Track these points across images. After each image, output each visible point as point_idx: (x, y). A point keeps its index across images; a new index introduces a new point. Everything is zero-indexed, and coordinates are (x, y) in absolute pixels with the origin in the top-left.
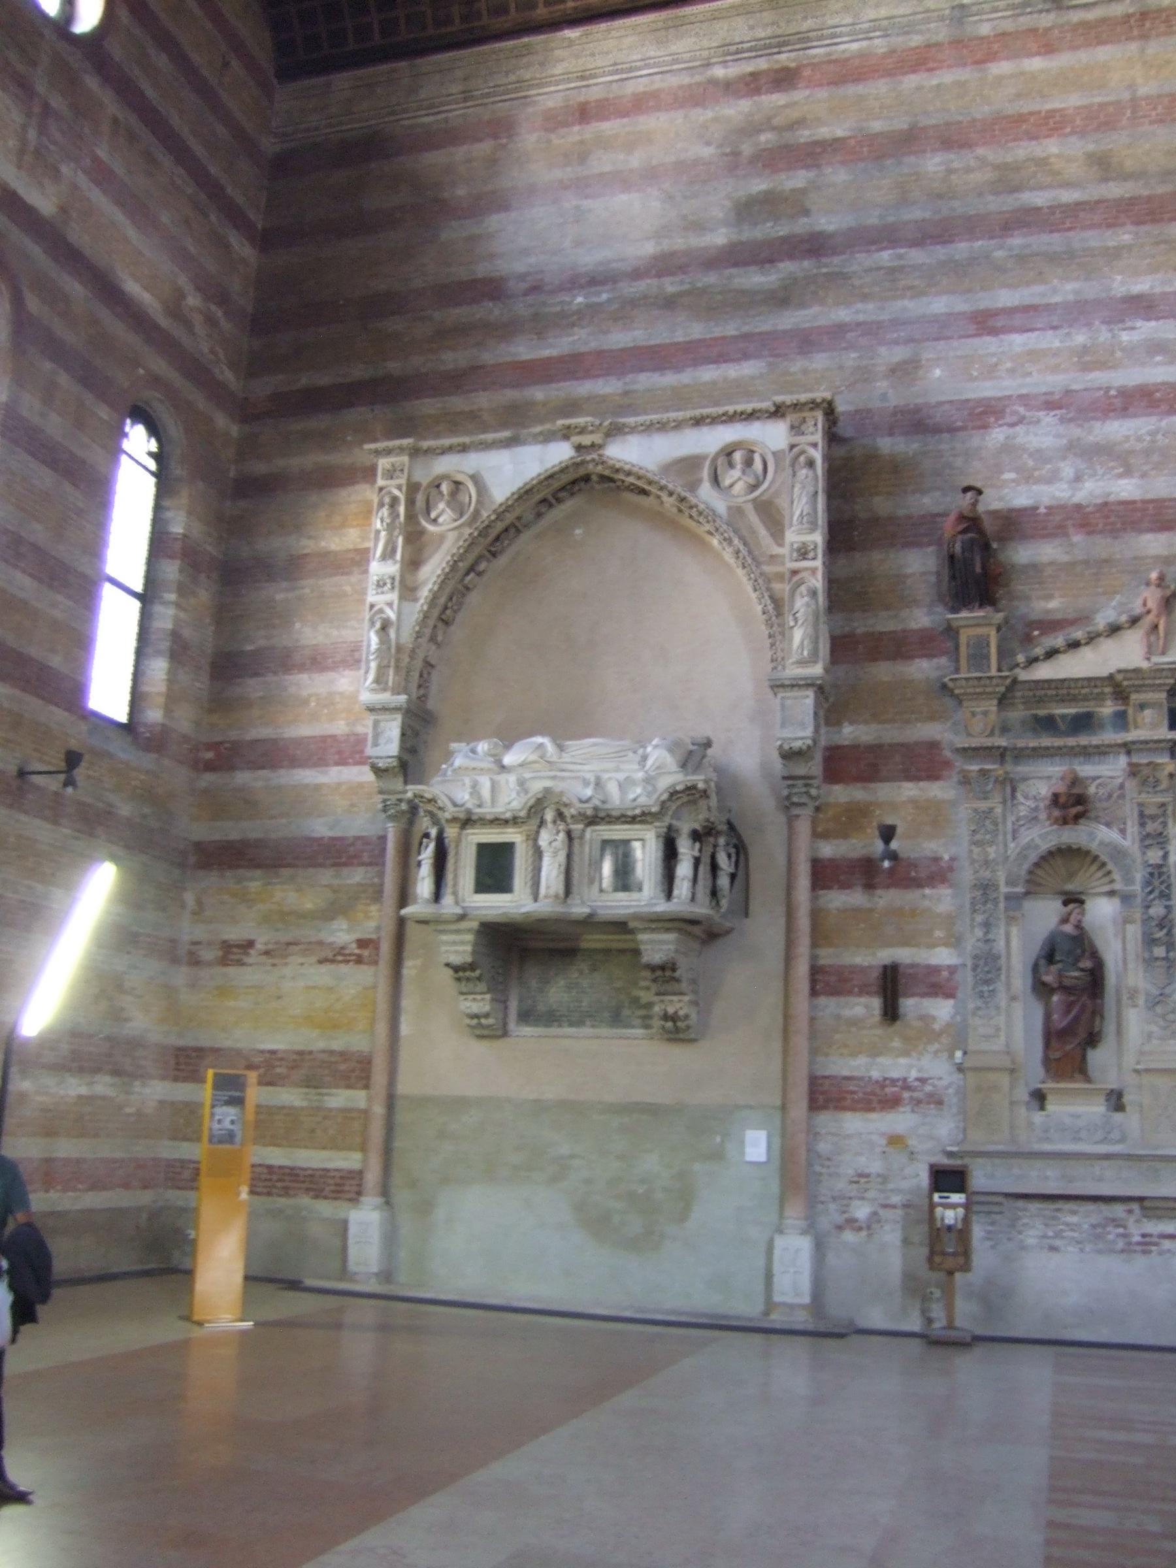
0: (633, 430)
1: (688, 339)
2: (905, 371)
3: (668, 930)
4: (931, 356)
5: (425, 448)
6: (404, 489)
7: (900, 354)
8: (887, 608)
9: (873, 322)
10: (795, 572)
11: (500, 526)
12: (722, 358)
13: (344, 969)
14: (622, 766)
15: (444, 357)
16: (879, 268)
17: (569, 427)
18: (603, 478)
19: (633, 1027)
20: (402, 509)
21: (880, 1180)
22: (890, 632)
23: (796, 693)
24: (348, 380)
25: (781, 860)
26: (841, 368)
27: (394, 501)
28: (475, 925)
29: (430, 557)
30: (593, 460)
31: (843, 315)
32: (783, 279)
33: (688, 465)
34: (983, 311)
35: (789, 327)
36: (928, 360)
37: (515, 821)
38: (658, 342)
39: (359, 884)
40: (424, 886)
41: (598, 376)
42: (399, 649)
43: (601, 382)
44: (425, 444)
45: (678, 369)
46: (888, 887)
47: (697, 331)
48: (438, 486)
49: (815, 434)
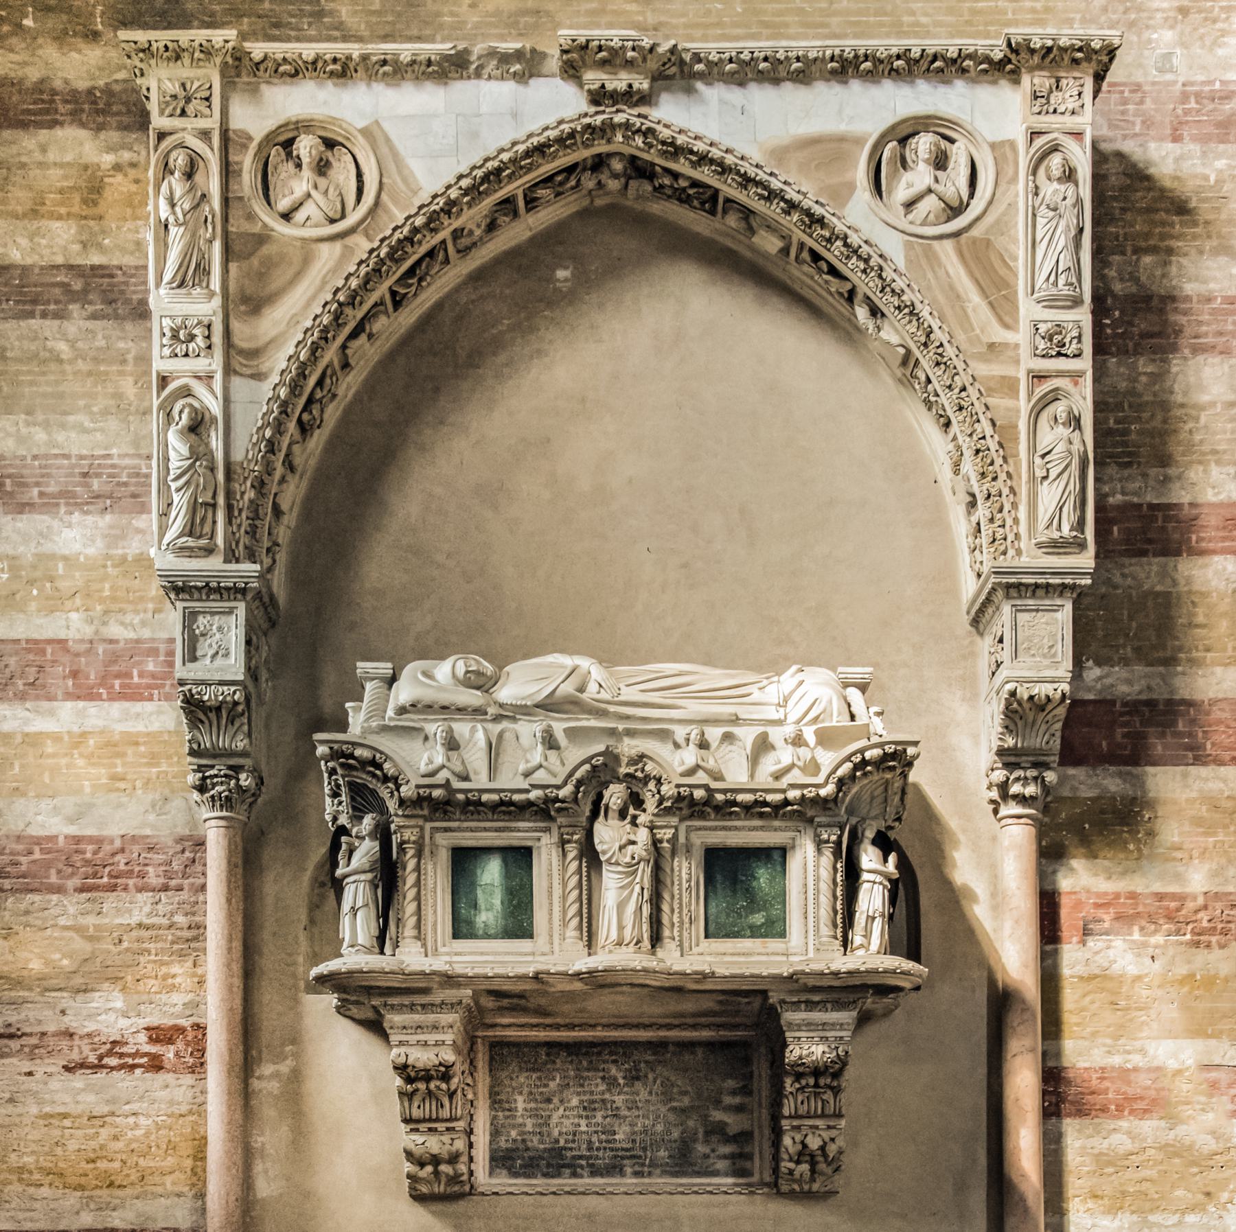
3: (839, 1005)
5: (257, 55)
10: (1039, 377)
13: (124, 1083)
19: (715, 1174)
30: (627, 126)
33: (826, 150)
37: (543, 810)
39: (140, 925)
44: (258, 49)
48: (288, 144)
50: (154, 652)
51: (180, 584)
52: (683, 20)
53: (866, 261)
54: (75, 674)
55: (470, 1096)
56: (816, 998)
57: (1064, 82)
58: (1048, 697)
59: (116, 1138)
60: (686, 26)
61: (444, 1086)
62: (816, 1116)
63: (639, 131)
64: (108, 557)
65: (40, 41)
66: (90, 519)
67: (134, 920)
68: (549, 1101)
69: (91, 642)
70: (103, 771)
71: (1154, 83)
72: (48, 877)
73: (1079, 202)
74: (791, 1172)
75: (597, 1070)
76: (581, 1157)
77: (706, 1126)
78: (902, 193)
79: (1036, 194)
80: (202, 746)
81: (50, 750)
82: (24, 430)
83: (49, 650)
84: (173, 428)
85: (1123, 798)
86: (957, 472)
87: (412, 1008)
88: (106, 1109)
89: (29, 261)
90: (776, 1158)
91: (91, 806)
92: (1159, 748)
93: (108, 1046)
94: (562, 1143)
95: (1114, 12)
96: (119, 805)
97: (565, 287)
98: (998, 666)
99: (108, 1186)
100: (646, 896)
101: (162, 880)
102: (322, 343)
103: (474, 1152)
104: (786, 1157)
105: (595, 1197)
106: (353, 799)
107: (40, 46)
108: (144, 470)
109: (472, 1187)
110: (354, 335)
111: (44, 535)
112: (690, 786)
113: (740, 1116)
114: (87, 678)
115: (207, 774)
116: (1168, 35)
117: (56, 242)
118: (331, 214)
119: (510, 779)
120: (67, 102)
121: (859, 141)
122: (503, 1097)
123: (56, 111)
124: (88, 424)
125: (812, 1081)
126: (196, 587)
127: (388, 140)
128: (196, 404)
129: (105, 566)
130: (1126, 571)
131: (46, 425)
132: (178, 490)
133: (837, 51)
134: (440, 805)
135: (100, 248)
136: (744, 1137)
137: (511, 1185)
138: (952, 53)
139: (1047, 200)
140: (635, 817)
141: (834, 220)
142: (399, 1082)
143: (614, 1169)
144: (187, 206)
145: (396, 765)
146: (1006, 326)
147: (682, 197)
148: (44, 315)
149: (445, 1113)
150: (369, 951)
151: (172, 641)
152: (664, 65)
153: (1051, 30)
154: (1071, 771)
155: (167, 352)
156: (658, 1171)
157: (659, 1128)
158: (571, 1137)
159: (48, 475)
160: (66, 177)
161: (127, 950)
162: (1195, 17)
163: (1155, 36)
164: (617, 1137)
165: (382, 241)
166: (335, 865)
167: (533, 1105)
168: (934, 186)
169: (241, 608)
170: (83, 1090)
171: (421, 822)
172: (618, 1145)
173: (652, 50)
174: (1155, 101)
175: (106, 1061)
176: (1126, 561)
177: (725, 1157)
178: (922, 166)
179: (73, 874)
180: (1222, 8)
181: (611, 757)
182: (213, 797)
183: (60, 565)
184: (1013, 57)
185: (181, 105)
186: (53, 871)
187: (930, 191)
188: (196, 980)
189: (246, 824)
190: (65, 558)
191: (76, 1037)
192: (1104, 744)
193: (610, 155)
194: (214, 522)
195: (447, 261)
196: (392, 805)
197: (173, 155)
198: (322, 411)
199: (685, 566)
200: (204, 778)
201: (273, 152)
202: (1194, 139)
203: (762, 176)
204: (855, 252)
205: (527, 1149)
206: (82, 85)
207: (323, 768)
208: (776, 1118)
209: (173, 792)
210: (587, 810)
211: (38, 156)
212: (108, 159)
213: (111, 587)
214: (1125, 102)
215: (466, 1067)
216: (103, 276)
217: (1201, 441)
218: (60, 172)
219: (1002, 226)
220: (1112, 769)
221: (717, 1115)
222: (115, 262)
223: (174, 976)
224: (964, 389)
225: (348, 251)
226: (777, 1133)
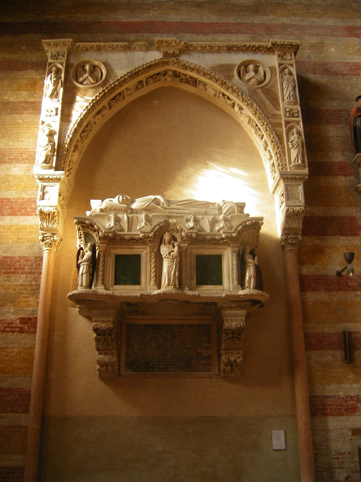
1: (209, 22)
3: (241, 308)
4: (329, 42)
7: (314, 40)
13: (11, 337)
15: (78, 15)
16: (301, 4)
21: (350, 456)
24: (25, 21)
27: (58, 71)
31: (285, 20)
34: (350, 27)
35: (260, 22)
36: (327, 44)
37: (142, 241)
38: (194, 21)
39: (21, 285)
51: (41, 177)
54: (11, 208)
58: (298, 211)
59: (6, 356)
61: (110, 337)
64: (25, 175)
67: (19, 283)
69: (17, 199)
70: (16, 237)
73: (294, 80)
78: (247, 77)
80: (44, 227)
83: (5, 201)
88: (4, 346)
89: (15, 101)
93: (7, 324)
99: (2, 373)
101: (29, 270)
102: (88, 113)
106: (85, 239)
110: (98, 113)
112: (191, 233)
115: (45, 236)
116: (309, 51)
121: (235, 66)
126: (45, 178)
129: (24, 178)
133: (228, 45)
140: (174, 244)
142: (95, 335)
147: (187, 82)
152: (183, 47)
154: (305, 238)
159: (12, 154)
163: (306, 51)
175: (7, 329)
179: (3, 268)
180: (321, 46)
181: (167, 223)
182: (46, 243)
183: (11, 178)
184: (273, 47)
188: (36, 302)
190: (13, 176)
195: (124, 97)
200: (44, 237)
201: (79, 68)
219: (275, 85)
223: (30, 301)
226: (219, 356)
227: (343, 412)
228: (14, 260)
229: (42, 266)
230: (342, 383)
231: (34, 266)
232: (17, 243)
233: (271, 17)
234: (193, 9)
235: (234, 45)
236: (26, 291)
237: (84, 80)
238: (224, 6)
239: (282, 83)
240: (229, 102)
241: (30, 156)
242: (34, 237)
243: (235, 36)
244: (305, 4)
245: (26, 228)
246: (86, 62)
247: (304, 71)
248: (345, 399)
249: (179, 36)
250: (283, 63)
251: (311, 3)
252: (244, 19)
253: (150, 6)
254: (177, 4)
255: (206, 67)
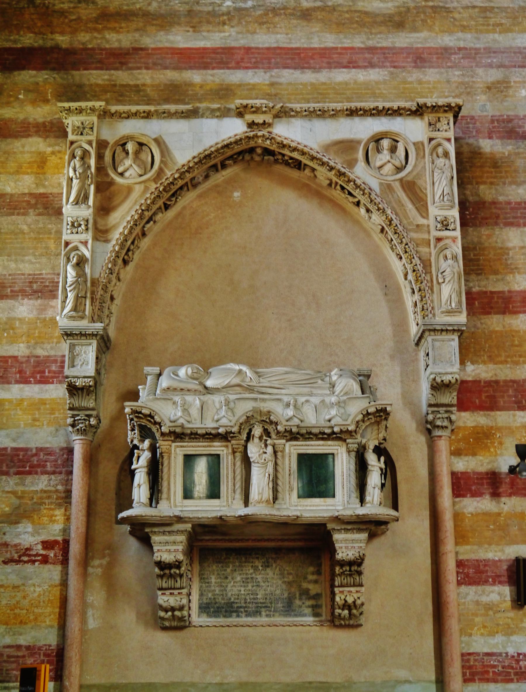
0: (297, 114)
1: (322, 46)
2: (498, 89)
3: (360, 530)
4: (518, 79)
5: (113, 111)
6: (94, 145)
7: (494, 75)
8: (496, 272)
9: (471, 49)
10: (439, 240)
11: (180, 183)
12: (351, 65)
13: (29, 568)
14: (315, 391)
16: (474, 7)
17: (246, 107)
18: (267, 151)
19: (305, 615)
20: (92, 162)
22: (499, 292)
23: (445, 336)
24: (19, 46)
25: (424, 472)
26: (448, 82)
27: (85, 154)
28: (188, 526)
29: (119, 205)
31: (448, 40)
32: (398, 7)
33: (346, 146)
37: (225, 437)
38: (297, 45)
39: (42, 491)
40: (140, 490)
41: (247, 68)
42: (94, 282)
43: (250, 72)
44: (113, 109)
45: (316, 69)
46: (510, 495)
47: (329, 40)
49: (448, 130)
50: (55, 361)
52: (286, 92)
53: (363, 191)
54: (20, 372)
55: (190, 576)
56: (349, 527)
57: (441, 119)
60: (288, 94)
61: (178, 572)
62: (351, 586)
63: (268, 138)
64: (38, 318)
65: (25, 103)
66: (31, 302)
68: (226, 578)
69: (28, 357)
71: (479, 116)
72: (2, 468)
74: (340, 615)
75: (249, 562)
76: (241, 607)
77: (300, 590)
79: (433, 163)
81: (7, 407)
82: (6, 263)
83: (10, 361)
84: (70, 264)
85: (487, 426)
86: (406, 279)
87: (164, 533)
88: (20, 583)
89: (14, 192)
90: (333, 608)
91: (23, 433)
92: (502, 403)
94: (232, 600)
95: (461, 88)
96: (36, 433)
97: (237, 200)
98: (427, 366)
100: (271, 479)
101: (53, 469)
102: (134, 227)
103: (191, 605)
104: (337, 607)
105: (248, 628)
106: (140, 432)
107: (25, 106)
108: (56, 280)
109: (190, 622)
110: (148, 222)
111: (12, 309)
112: (290, 426)
113: (317, 586)
114: (26, 373)
116: (484, 97)
117: (24, 184)
118: (140, 173)
119: (209, 424)
120: (34, 127)
121: (359, 142)
122: (205, 576)
123: (29, 131)
124: (34, 260)
125: (348, 568)
126: (76, 334)
127: (164, 142)
128: (80, 253)
129: (36, 323)
130: (482, 321)
131: (16, 261)
132: (70, 291)
133: (349, 107)
134: (179, 435)
135: (44, 186)
136: (317, 596)
137: (208, 622)
138: (395, 108)
139: (438, 166)
140: (266, 440)
141: (350, 174)
142: (157, 570)
143: (257, 613)
144: (81, 171)
145: (160, 417)
146: (423, 217)
148: (18, 214)
149: (178, 585)
150: (145, 505)
151: (64, 356)
153: (436, 100)
155: (69, 231)
156: (277, 614)
157: (278, 592)
158: (236, 597)
160: (32, 157)
161: (35, 503)
162: (494, 90)
163: (478, 98)
164: (258, 597)
165: (161, 184)
166: (132, 464)
167: (219, 580)
168: (390, 160)
169: (95, 343)
170: (11, 573)
171: (170, 443)
172: (259, 601)
173: (273, 107)
174: (481, 123)
176: (482, 317)
177: (309, 607)
178: (385, 152)
180: (504, 87)
183: (17, 323)
185: (80, 131)
186: (4, 465)
187: (389, 162)
189: (92, 442)
190: (20, 319)
191: (9, 547)
192: (477, 401)
193: (256, 147)
194: (85, 305)
195: (188, 190)
196: (158, 435)
197: (77, 150)
198: (133, 254)
199: (289, 320)
200: (75, 421)
201: (118, 148)
202: (498, 138)
203: (319, 156)
204: (359, 187)
205: (216, 603)
206: (41, 120)
207: (128, 418)
208: (333, 586)
209: (60, 426)
210: (244, 436)
211: (21, 149)
212: (49, 150)
213: (39, 332)
214: (468, 123)
215: (188, 561)
216: (44, 197)
217: (511, 264)
218: (29, 155)
219: (419, 176)
220: (481, 413)
221: (305, 585)
222: (49, 192)
224: (407, 244)
225: (146, 189)
226: (333, 594)
227: (513, 676)
228: (29, 453)
229: (73, 461)
230: (512, 634)
231: (59, 462)
232: (33, 426)
233: (424, 34)
234: (295, 21)
235: (359, 107)
236: (50, 501)
237: (125, 171)
238: (347, 16)
239: (433, 172)
240: (351, 199)
241: (45, 286)
242: (58, 417)
243: (365, 73)
244: (481, 7)
245: (45, 404)
246: (130, 138)
247: (474, 133)
248: (516, 658)
249: (273, 74)
250: (434, 136)
251: (492, 4)
252: (380, 40)
253: (225, 17)
254: (270, 13)
255: (315, 147)
